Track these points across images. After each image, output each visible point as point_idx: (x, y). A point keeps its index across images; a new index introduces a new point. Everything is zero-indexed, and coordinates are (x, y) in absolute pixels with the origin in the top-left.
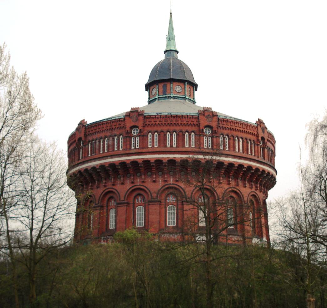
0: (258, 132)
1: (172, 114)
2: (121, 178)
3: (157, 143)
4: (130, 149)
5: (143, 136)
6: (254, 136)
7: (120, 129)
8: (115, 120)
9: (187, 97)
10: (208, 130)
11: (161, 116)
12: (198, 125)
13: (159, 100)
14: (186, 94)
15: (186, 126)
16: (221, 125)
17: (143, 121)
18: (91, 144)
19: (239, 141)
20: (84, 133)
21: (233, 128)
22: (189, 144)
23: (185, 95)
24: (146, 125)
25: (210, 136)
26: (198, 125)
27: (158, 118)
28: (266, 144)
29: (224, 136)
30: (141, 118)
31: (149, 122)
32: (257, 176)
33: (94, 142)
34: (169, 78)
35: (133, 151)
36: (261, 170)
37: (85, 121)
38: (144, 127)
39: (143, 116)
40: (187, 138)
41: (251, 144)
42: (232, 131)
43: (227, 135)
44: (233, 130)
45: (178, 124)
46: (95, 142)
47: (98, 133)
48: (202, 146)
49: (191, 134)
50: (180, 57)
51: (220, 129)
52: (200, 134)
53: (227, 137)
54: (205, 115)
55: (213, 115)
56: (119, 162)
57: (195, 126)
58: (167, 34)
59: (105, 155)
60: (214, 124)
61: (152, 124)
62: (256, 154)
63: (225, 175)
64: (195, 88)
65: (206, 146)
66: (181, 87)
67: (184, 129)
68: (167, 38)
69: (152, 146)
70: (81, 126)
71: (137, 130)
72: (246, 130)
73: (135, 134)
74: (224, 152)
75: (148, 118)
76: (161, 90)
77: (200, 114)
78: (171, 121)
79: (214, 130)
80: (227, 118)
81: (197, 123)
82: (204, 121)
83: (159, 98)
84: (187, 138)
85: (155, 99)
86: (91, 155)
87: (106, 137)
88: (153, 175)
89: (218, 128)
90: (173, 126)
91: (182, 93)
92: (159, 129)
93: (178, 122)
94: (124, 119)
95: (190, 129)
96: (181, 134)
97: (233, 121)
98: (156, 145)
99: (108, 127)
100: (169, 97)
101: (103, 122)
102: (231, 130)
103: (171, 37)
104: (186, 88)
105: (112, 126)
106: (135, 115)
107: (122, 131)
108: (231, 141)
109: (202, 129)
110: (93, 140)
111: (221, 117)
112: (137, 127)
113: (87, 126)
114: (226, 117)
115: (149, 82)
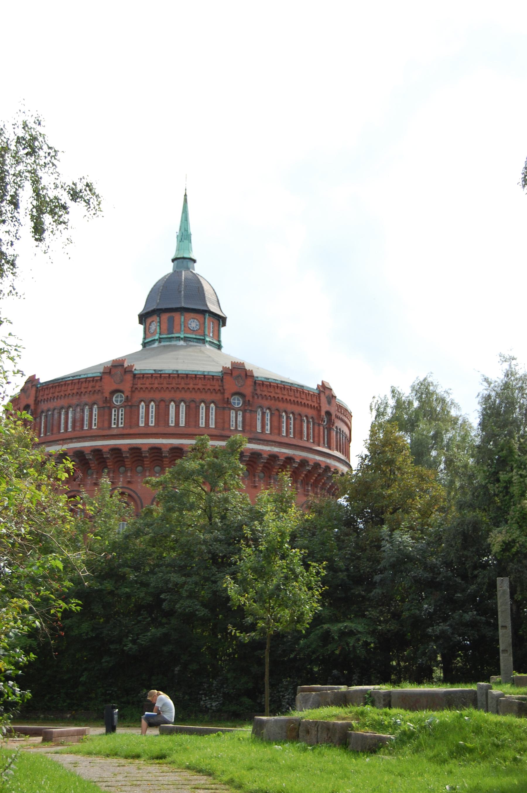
0: (320, 403)
1: (179, 372)
2: (93, 474)
3: (154, 419)
4: (110, 427)
5: (131, 406)
6: (313, 410)
7: (94, 393)
8: (86, 378)
9: (208, 339)
10: (238, 400)
11: (161, 374)
12: (222, 391)
13: (160, 342)
14: (207, 333)
15: (201, 392)
16: (259, 392)
17: (132, 382)
18: (46, 416)
19: (288, 418)
20: (34, 399)
21: (278, 397)
22: (206, 422)
23: (204, 335)
24: (136, 388)
25: (240, 410)
26: (222, 391)
27: (156, 378)
28: (334, 423)
29: (263, 409)
30: (129, 377)
31: (142, 384)
32: (325, 478)
33: (50, 413)
34: (179, 306)
35: (115, 432)
36: (323, 466)
37: (37, 378)
38: (132, 392)
39: (132, 375)
40: (202, 412)
41: (308, 422)
42: (277, 402)
43: (269, 408)
44: (279, 401)
45: (189, 388)
46: (53, 414)
47: (57, 399)
48: (226, 426)
49: (209, 407)
50: (198, 269)
51: (258, 398)
52: (224, 406)
53: (268, 411)
54: (233, 375)
55: (246, 375)
56: (92, 448)
57: (216, 393)
58: (178, 231)
59: (67, 436)
60: (248, 390)
61: (147, 388)
62: (316, 439)
63: (264, 474)
64: (221, 323)
65: (234, 426)
66: (199, 322)
67: (198, 397)
68: (177, 236)
69: (145, 424)
70: (30, 385)
71: (121, 397)
72: (300, 400)
73: (119, 404)
74: (262, 437)
75: (139, 378)
76: (165, 326)
77: (225, 373)
78: (176, 384)
79: (247, 399)
80: (270, 381)
81: (221, 388)
82: (230, 386)
83: (160, 338)
84: (202, 412)
85: (154, 340)
86: (45, 434)
87: (70, 407)
88: (146, 470)
89: (253, 397)
90: (180, 391)
91: (199, 331)
92: (158, 396)
93: (188, 386)
94: (101, 378)
95: (208, 397)
96: (193, 405)
97: (279, 385)
98: (152, 423)
99: (74, 389)
100: (177, 337)
101: (66, 381)
102: (275, 400)
103: (184, 236)
104: (207, 323)
105: (80, 389)
106: (119, 371)
107: (97, 397)
108: (275, 418)
109: (228, 398)
110: (48, 410)
111: (259, 379)
112: (122, 392)
113: (39, 386)
114: (268, 379)
115: (145, 312)
